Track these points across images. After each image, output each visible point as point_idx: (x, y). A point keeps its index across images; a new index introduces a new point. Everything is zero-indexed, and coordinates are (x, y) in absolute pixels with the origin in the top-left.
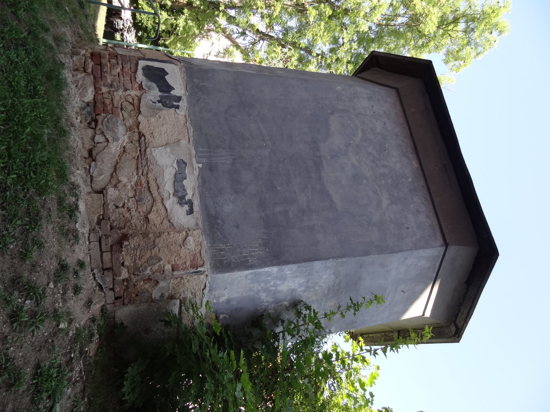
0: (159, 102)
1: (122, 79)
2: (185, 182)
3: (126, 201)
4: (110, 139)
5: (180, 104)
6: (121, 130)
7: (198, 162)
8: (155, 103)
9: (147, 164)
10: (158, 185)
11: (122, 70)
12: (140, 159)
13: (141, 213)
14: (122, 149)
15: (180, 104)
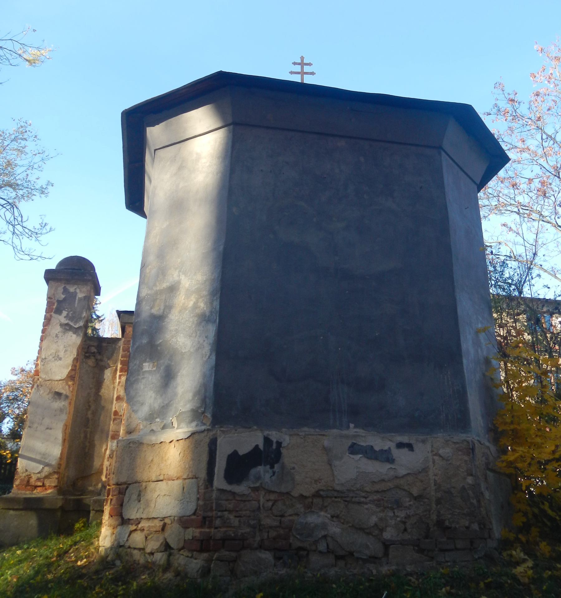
0: (272, 467)
1: (244, 513)
2: (377, 448)
3: (398, 519)
4: (323, 533)
5: (275, 440)
6: (312, 519)
7: (348, 427)
8: (274, 473)
9: (353, 491)
10: (380, 481)
11: (230, 511)
12: (348, 499)
13: (411, 503)
14: (334, 519)
15: (275, 440)
